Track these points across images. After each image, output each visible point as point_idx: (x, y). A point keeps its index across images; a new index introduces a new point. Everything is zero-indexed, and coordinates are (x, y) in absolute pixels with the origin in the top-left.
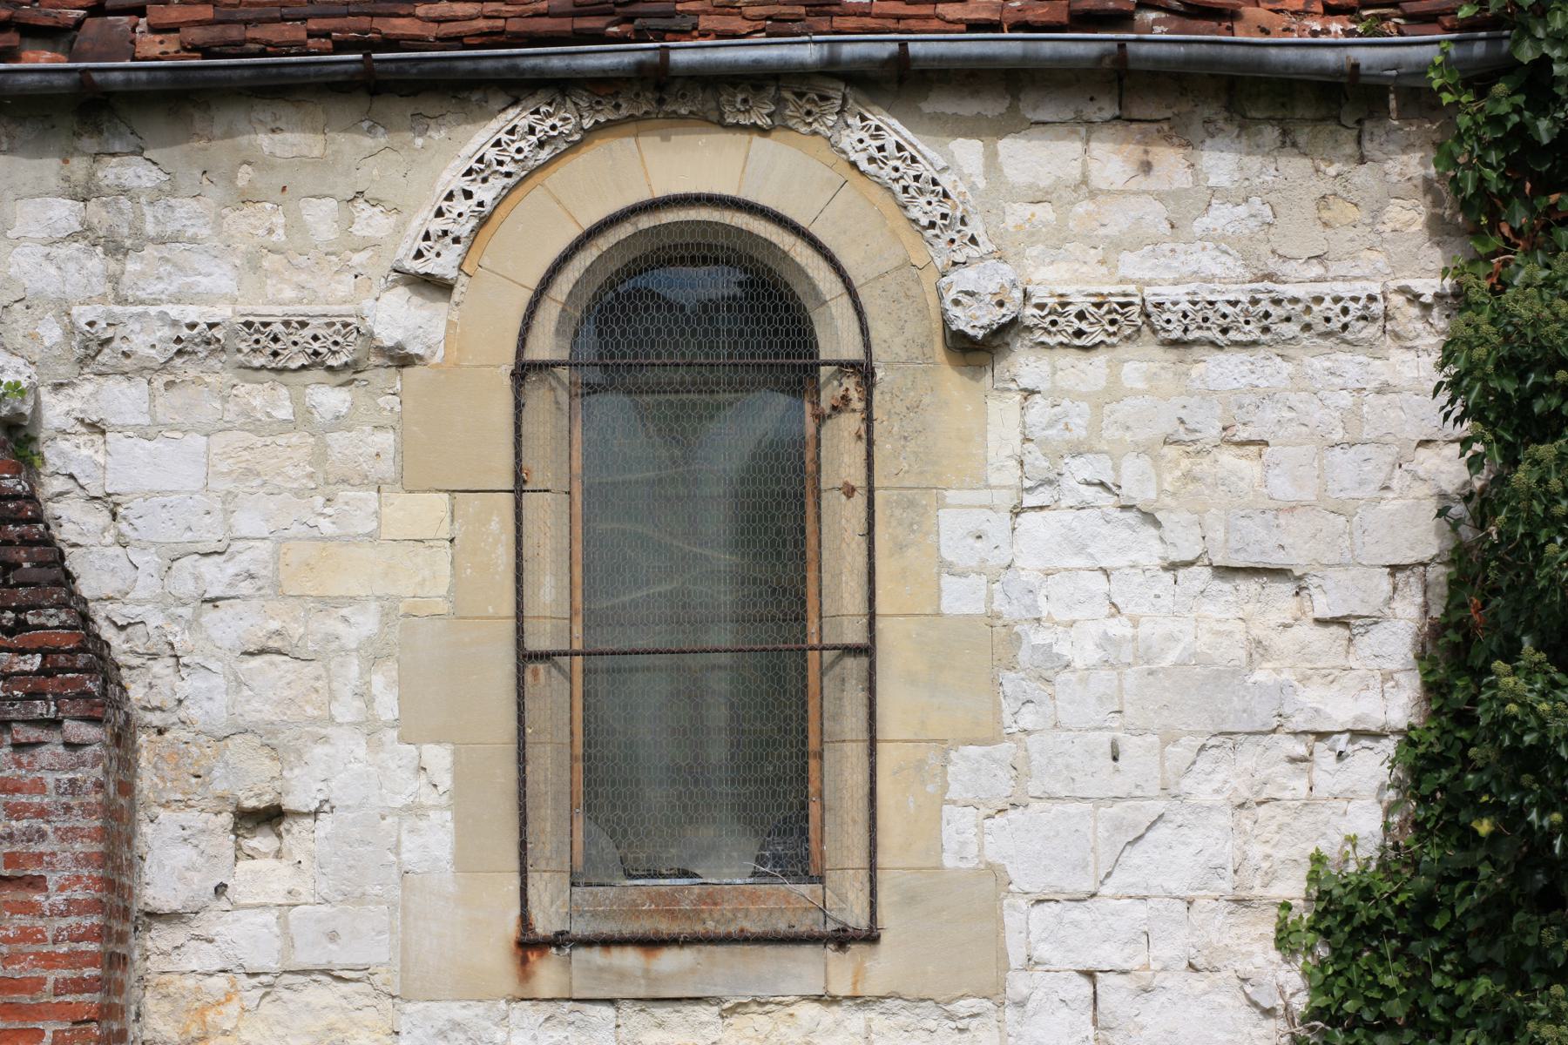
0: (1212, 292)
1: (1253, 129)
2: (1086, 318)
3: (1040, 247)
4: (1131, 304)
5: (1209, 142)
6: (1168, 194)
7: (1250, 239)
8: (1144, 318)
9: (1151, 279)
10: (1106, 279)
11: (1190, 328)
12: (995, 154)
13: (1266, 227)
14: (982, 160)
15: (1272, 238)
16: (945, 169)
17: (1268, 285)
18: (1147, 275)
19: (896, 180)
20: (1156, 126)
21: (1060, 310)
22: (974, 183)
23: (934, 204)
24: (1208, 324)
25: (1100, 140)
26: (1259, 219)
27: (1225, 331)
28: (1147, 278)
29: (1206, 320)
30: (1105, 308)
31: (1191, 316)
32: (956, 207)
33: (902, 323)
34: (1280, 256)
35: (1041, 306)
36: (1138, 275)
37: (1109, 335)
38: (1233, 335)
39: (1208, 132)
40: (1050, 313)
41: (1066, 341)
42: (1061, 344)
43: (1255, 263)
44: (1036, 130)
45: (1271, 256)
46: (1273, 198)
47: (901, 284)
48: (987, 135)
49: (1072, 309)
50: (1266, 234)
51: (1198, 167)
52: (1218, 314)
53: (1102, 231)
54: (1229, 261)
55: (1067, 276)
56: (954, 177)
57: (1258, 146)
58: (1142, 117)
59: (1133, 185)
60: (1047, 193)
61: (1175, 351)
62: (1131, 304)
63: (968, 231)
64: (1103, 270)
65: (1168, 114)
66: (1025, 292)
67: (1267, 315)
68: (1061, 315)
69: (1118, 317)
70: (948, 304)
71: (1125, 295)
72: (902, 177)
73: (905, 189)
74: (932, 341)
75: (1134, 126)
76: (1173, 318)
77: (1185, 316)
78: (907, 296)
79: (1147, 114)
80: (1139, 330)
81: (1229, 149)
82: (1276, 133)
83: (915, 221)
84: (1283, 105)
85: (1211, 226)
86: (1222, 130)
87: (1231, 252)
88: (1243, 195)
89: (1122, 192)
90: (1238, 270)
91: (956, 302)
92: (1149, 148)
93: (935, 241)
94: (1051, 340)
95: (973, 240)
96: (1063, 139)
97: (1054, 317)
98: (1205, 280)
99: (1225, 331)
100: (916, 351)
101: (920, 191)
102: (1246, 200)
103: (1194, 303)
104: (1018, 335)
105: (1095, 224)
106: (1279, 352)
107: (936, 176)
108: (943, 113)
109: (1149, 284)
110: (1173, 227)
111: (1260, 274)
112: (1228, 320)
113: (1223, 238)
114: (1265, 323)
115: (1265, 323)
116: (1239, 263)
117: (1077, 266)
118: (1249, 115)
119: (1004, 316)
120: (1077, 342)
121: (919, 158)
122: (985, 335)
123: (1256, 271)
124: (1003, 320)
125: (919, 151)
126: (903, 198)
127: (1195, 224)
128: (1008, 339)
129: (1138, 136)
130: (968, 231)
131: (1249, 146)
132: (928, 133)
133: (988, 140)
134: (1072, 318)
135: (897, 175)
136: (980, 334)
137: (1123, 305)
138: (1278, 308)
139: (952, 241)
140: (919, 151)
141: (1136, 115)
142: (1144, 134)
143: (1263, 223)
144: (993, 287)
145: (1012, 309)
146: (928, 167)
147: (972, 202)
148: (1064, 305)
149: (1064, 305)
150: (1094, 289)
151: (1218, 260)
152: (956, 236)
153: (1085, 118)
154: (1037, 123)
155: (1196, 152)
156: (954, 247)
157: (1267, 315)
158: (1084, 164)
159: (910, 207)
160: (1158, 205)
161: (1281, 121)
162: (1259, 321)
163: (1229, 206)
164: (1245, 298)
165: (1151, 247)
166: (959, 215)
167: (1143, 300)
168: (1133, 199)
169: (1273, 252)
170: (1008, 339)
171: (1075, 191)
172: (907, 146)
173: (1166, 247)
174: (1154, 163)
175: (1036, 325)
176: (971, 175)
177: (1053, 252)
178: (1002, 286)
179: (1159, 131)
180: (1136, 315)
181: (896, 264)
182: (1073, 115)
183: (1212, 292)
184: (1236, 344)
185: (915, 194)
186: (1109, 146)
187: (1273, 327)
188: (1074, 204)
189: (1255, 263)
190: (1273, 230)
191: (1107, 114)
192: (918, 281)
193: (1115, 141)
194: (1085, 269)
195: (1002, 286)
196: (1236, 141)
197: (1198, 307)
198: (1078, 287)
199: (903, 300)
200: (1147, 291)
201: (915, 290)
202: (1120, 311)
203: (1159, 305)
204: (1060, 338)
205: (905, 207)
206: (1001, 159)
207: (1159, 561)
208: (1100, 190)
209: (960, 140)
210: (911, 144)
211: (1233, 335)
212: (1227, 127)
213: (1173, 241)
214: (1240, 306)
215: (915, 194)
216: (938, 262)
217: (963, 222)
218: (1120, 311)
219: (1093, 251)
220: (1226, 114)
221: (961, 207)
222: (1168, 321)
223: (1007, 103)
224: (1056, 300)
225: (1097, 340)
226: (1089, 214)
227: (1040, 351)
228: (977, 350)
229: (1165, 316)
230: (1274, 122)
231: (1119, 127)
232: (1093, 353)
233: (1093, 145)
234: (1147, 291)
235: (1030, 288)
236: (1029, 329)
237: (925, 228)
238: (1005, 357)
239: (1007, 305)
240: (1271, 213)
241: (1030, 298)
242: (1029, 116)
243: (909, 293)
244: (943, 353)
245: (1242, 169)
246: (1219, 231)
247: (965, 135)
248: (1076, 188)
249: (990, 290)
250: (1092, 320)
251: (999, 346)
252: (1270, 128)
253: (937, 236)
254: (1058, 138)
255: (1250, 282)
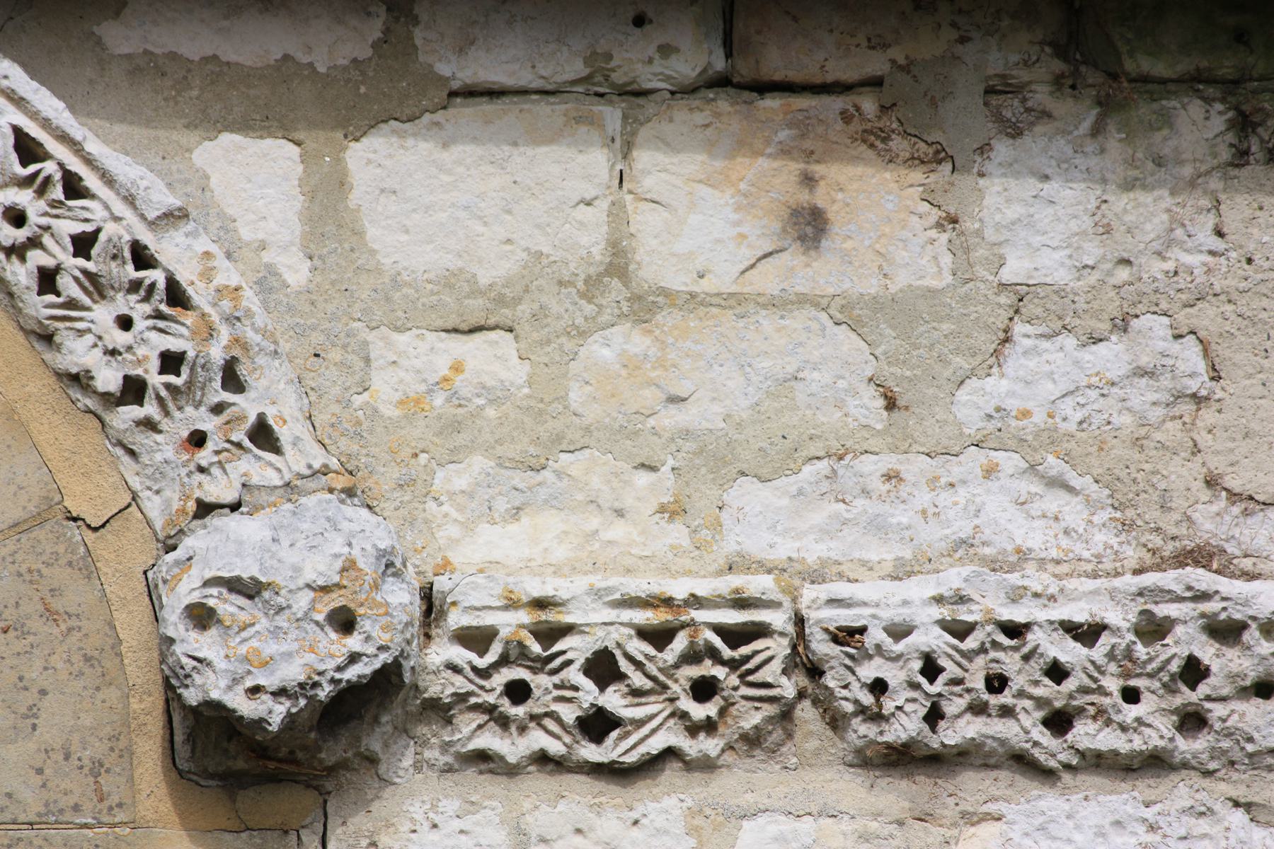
0: (1015, 596)
1: (1144, 110)
2: (621, 677)
3: (479, 463)
4: (759, 631)
5: (1003, 149)
6: (876, 304)
7: (1138, 443)
8: (803, 681)
9: (824, 563)
10: (687, 563)
11: (950, 708)
12: (342, 183)
13: (1186, 408)
14: (298, 202)
15: (1204, 439)
16: (175, 217)
17: (1201, 578)
18: (814, 551)
19: (17, 251)
20: (837, 103)
21: (536, 648)
22: (272, 270)
23: (140, 324)
24: (1006, 698)
25: (667, 145)
26: (1166, 382)
27: (1059, 722)
28: (811, 559)
29: (997, 683)
30: (680, 643)
31: (951, 670)
32: (211, 332)
33: (31, 697)
34: (1234, 496)
35: (476, 639)
36: (783, 550)
37: (694, 729)
38: (1086, 734)
39: (999, 118)
40: (504, 661)
41: (555, 747)
42: (543, 759)
43: (1153, 514)
44: (465, 112)
45: (1205, 495)
46: (1207, 317)
47: (32, 577)
48: (312, 125)
49: (577, 648)
50: (1188, 427)
51: (969, 225)
52: (1035, 668)
53: (671, 418)
54: (1073, 511)
55: (561, 553)
56: (203, 244)
57: (1159, 162)
58: (793, 75)
59: (768, 280)
60: (501, 301)
61: (904, 784)
62: (759, 631)
63: (248, 406)
64: (677, 533)
65: (876, 64)
66: (427, 595)
67: (1194, 672)
68: (540, 664)
69: (720, 672)
70: (174, 624)
71: (741, 603)
72: (34, 242)
73: (47, 280)
74: (128, 753)
75: (772, 103)
76: (894, 676)
77: (931, 669)
78: (50, 614)
79: (806, 67)
80: (786, 715)
81: (1066, 169)
82: (1218, 123)
83: (80, 380)
84: (1240, 37)
85: (1012, 404)
86: (1046, 115)
87: (1076, 482)
88: (1113, 309)
89: (733, 301)
90: (1101, 538)
91: (201, 616)
92: (818, 169)
93: (142, 440)
94: (511, 748)
95: (263, 435)
96: (551, 139)
97: (520, 673)
98: (995, 565)
99: (1059, 722)
100: (75, 786)
101: (96, 286)
102: (1122, 325)
103: (960, 631)
104: (403, 730)
105: (650, 397)
106: (1240, 793)
107: (146, 238)
108: (173, 56)
109: (816, 577)
110: (891, 404)
111: (1169, 548)
112: (1070, 685)
113: (1052, 438)
114: (1188, 696)
115: (1188, 696)
116: (1103, 516)
117: (594, 522)
118: (1129, 65)
119: (354, 658)
120: (591, 752)
121: (91, 181)
122: (290, 719)
123: (1157, 541)
124: (352, 674)
125: (89, 161)
126: (39, 306)
127: (962, 395)
128: (374, 744)
129: (783, 135)
130: (248, 406)
131: (1131, 163)
132: (130, 114)
133: (314, 139)
134: (574, 675)
135: (21, 235)
136: (276, 713)
137: (734, 636)
138: (1232, 653)
139: (198, 440)
140: (89, 161)
141: (775, 64)
142: (803, 126)
143: (1179, 396)
144: (320, 568)
145: (384, 638)
146: (120, 208)
147: (261, 319)
148: (550, 634)
149: (550, 634)
150: (640, 586)
151: (1036, 507)
152: (209, 424)
153: (619, 78)
154: (471, 93)
155: (965, 182)
156: (205, 456)
157: (1194, 672)
158: (617, 214)
159: (65, 337)
160: (846, 340)
161: (1230, 86)
162: (1170, 689)
163: (1069, 341)
164: (1120, 617)
165: (823, 466)
166: (217, 353)
167: (800, 621)
168: (767, 321)
169: (1212, 482)
170: (374, 744)
171: (587, 296)
172: (51, 145)
173: (871, 467)
174: (833, 212)
175: (461, 698)
176: (263, 246)
177: (520, 479)
178: (349, 566)
179: (846, 117)
180: (776, 666)
181: (16, 514)
182: (577, 68)
183: (1015, 596)
184: (1097, 762)
185: (75, 292)
186: (692, 163)
187: (1217, 711)
188: (583, 334)
189: (1153, 514)
190: (1208, 416)
191: (686, 67)
192: (88, 567)
193: (710, 147)
194: (619, 531)
195: (349, 566)
196: (1090, 147)
197: (971, 643)
198: (598, 581)
199: (35, 624)
200: (810, 593)
201: (76, 595)
202: (727, 653)
203: (847, 636)
204: (538, 740)
205: (48, 338)
206: (354, 198)
207: (84, 808)
208: (664, 292)
209: (228, 139)
210: (64, 138)
211: (1086, 734)
212: (1062, 107)
213: (894, 449)
214: (1105, 640)
215: (75, 292)
216: (154, 507)
217: (232, 379)
218: (727, 653)
219: (644, 478)
220: (1058, 66)
221: (224, 334)
222: (879, 687)
223: (374, 30)
224: (524, 617)
225: (656, 745)
226: (631, 365)
227: (474, 781)
228: (275, 779)
229: (868, 671)
230: (1211, 91)
231: (723, 105)
232: (642, 788)
233: (644, 158)
234: (810, 593)
235: (442, 584)
236: (440, 711)
237: (111, 400)
238: (363, 804)
239: (365, 625)
240: (1201, 366)
241: (443, 614)
242: (444, 69)
243: (56, 604)
244: (162, 790)
245: (1108, 230)
246: (1039, 418)
247: (244, 126)
248: (592, 288)
249: (309, 576)
250: (638, 680)
251: (343, 765)
252: (1196, 108)
253: (149, 425)
254: (538, 138)
255: (1137, 572)
